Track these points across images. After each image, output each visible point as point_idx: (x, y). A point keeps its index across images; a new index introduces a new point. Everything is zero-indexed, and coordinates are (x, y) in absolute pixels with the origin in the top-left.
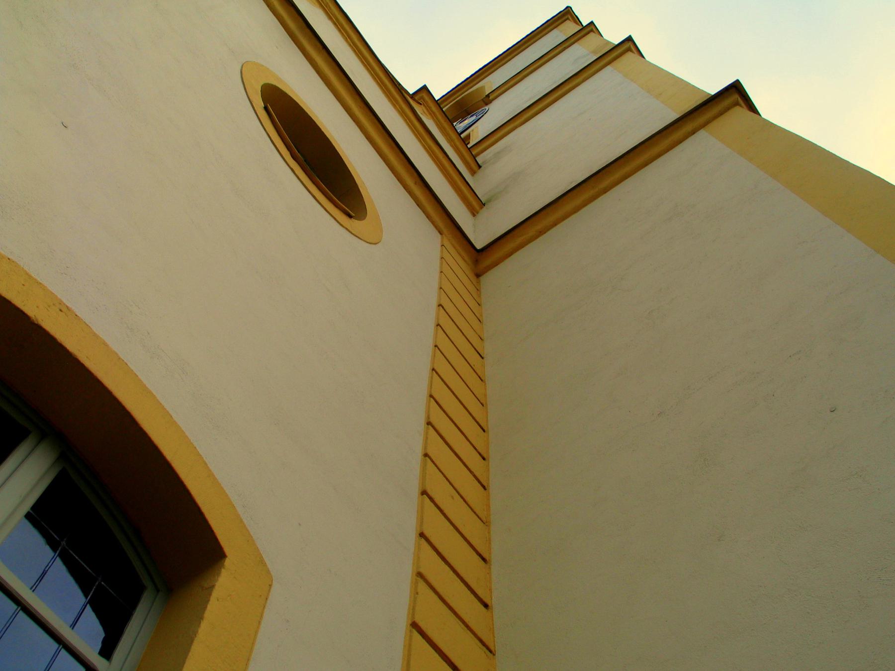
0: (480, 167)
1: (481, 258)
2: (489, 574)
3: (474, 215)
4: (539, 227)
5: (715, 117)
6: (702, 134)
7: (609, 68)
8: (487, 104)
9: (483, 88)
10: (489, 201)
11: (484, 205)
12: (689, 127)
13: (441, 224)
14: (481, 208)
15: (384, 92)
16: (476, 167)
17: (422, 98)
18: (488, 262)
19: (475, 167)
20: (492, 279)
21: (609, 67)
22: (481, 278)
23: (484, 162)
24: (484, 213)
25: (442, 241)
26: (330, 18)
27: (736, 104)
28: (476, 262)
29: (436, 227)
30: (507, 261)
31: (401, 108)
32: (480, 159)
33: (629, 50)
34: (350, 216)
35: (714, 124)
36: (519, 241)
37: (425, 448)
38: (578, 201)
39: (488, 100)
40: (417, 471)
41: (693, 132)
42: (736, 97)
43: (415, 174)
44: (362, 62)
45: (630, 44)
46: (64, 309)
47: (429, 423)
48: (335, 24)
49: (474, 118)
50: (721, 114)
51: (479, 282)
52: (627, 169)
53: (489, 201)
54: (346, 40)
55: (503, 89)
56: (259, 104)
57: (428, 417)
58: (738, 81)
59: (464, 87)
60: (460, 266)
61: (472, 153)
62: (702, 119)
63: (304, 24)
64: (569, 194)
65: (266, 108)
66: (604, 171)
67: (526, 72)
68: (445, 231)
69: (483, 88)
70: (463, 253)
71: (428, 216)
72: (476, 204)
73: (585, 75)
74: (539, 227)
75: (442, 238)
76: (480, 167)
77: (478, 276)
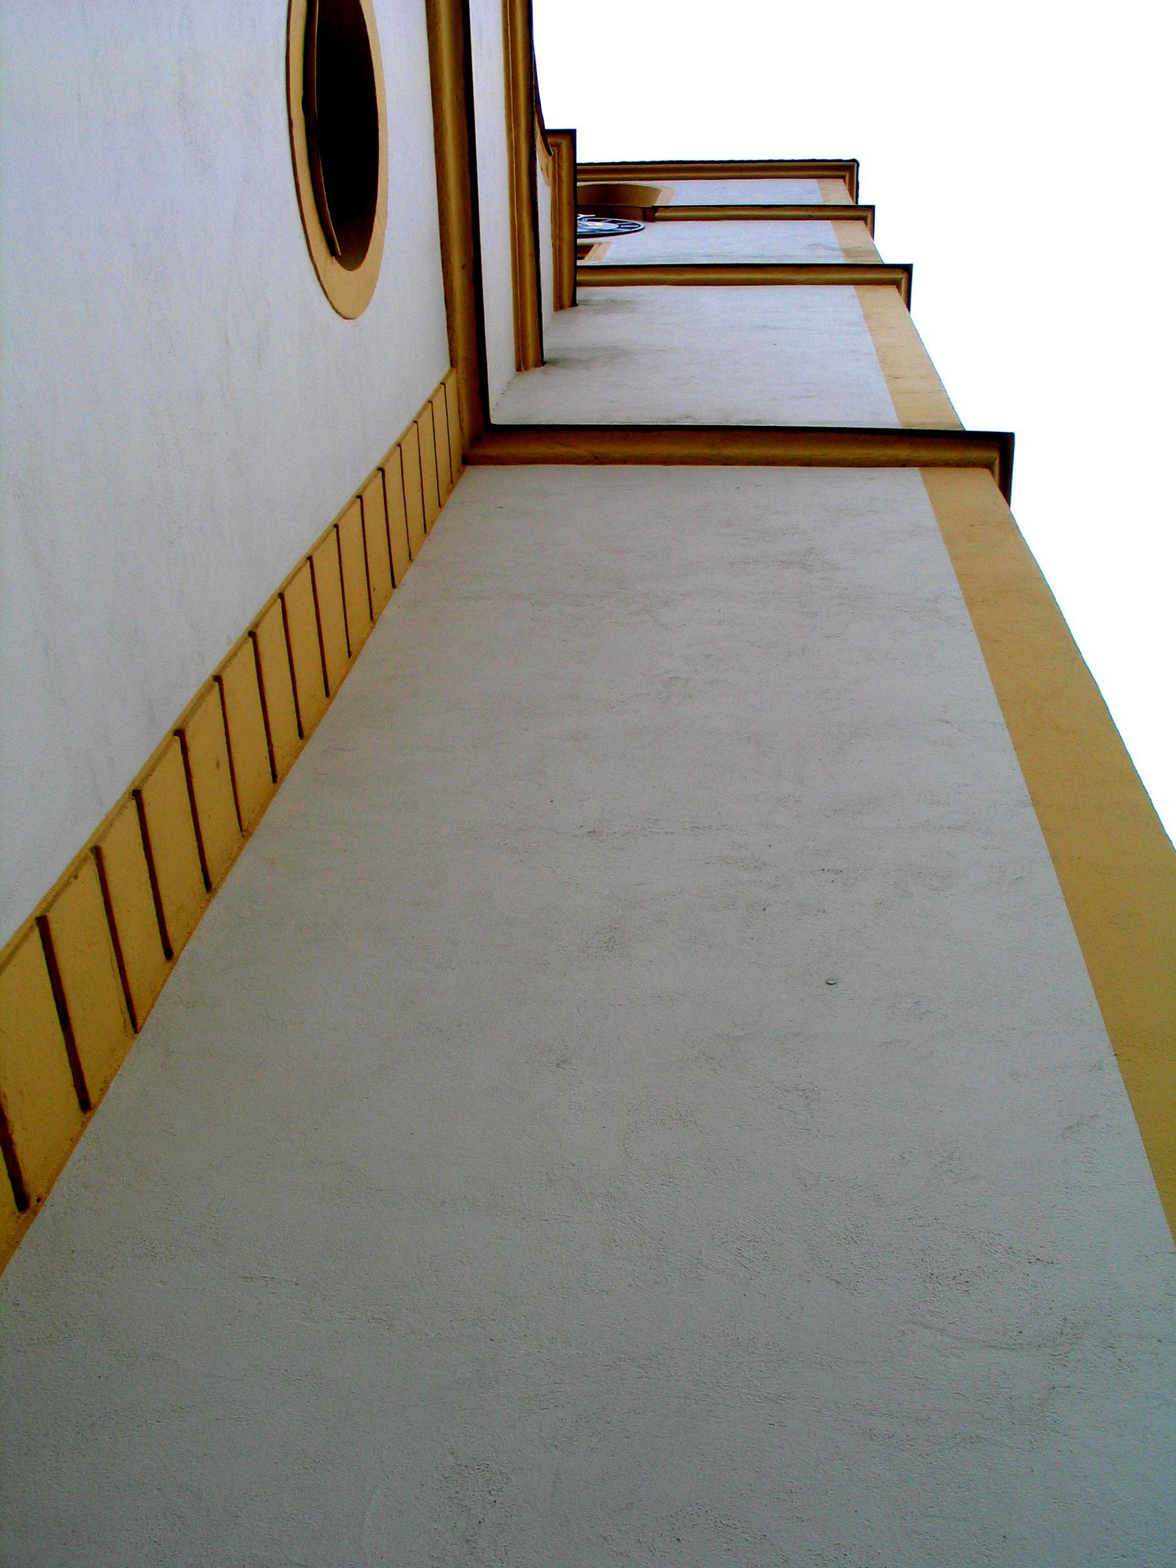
0: (574, 303)
1: (485, 440)
2: (203, 909)
3: (519, 369)
9: (656, 191)
10: (554, 363)
16: (566, 301)
17: (558, 146)
19: (566, 299)
20: (486, 482)
22: (469, 468)
23: (586, 302)
25: (447, 376)
32: (581, 293)
36: (560, 450)
39: (651, 214)
41: (904, 464)
42: (994, 455)
49: (614, 226)
51: (460, 472)
53: (554, 363)
55: (673, 214)
60: (448, 430)
69: (656, 191)
72: (531, 354)
75: (450, 372)
76: (574, 303)
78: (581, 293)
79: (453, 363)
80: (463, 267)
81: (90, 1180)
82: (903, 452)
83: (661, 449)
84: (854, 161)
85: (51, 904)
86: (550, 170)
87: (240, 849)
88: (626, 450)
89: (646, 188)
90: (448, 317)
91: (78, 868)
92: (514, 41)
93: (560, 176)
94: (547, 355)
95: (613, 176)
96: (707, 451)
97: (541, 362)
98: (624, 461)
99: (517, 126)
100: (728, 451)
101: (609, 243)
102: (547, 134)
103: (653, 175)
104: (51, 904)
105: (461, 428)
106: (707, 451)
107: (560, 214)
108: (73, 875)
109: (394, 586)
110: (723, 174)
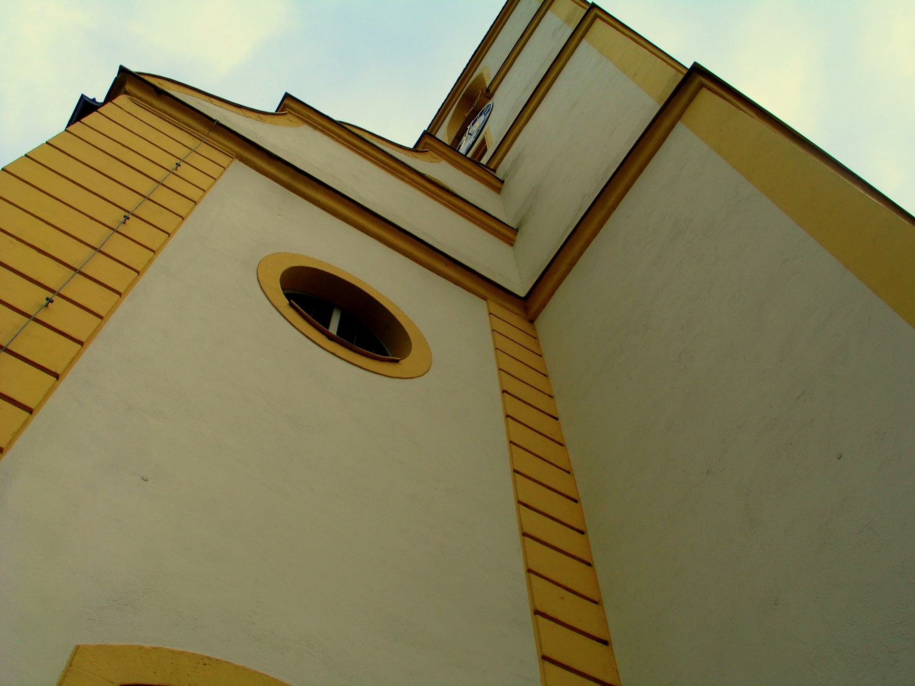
0: (502, 182)
1: (528, 305)
2: (613, 654)
3: (512, 245)
4: (568, 260)
6: (680, 127)
7: (584, 42)
8: (490, 98)
10: (520, 225)
11: (517, 230)
12: (667, 123)
13: (482, 291)
14: (516, 235)
15: (389, 171)
16: (497, 185)
17: (427, 144)
18: (535, 306)
23: (505, 175)
24: (520, 239)
25: (488, 308)
26: (316, 128)
27: (702, 86)
28: (526, 309)
32: (500, 174)
33: (596, 16)
34: (397, 361)
36: (556, 277)
37: (526, 563)
39: (489, 94)
40: (524, 588)
41: (672, 126)
45: (596, 11)
46: (207, 661)
47: (524, 534)
49: (482, 118)
50: (691, 100)
51: (534, 329)
52: (626, 180)
53: (520, 225)
55: (497, 82)
56: (283, 301)
58: (695, 63)
59: (464, 79)
60: (512, 317)
62: (676, 111)
64: (584, 220)
65: (291, 305)
66: (607, 189)
67: (514, 55)
68: (488, 295)
69: (481, 75)
70: (509, 306)
71: (469, 290)
72: (507, 233)
73: (565, 56)
74: (568, 260)
75: (488, 304)
76: (502, 182)
77: (532, 321)
78: (500, 174)
79: (485, 299)
81: (7, 456)
83: (587, 232)
85: (522, 528)
86: (436, 156)
87: (604, 612)
89: (477, 78)
91: (544, 669)
92: (372, 156)
94: (513, 225)
96: (603, 213)
97: (516, 231)
98: (581, 253)
102: (417, 149)
104: (522, 528)
106: (603, 213)
108: (507, 424)
109: (557, 419)
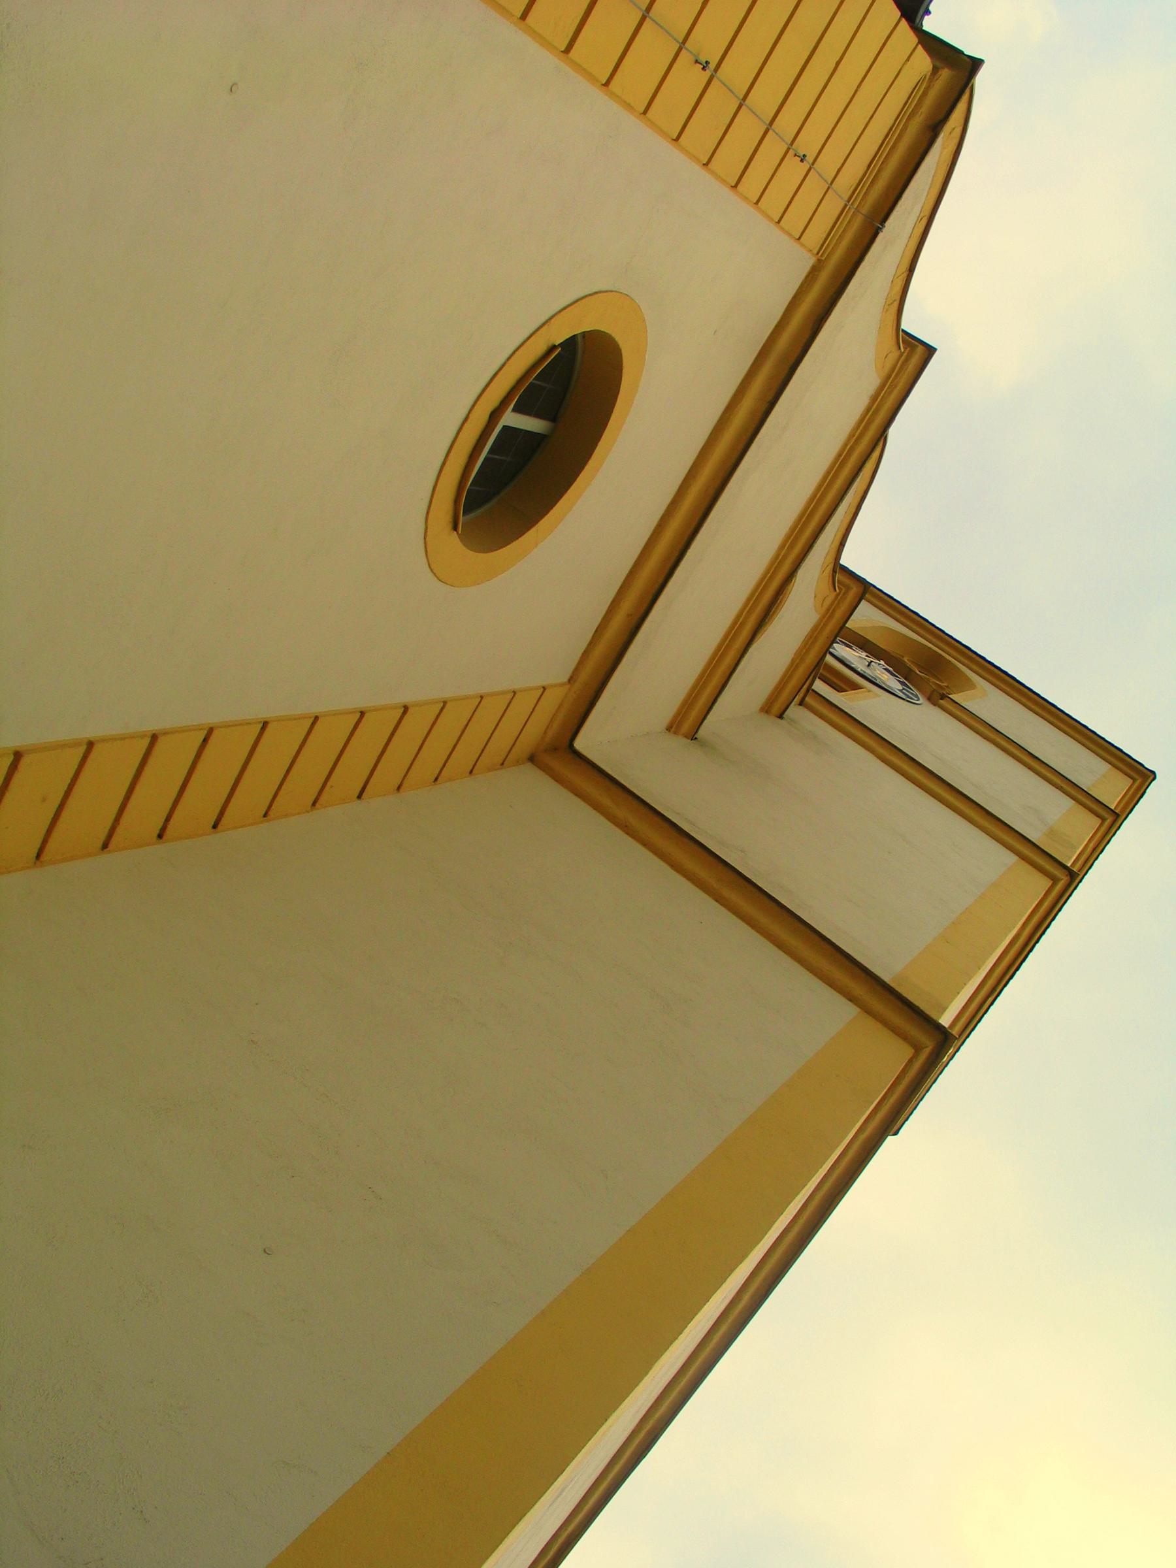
0: (781, 716)
1: (560, 752)
5: (885, 1023)
6: (851, 1011)
8: (929, 699)
9: (968, 685)
10: (704, 744)
11: (694, 738)
13: (584, 676)
17: (848, 588)
19: (776, 708)
20: (533, 781)
21: (1015, 858)
22: (529, 765)
24: (678, 743)
26: (874, 399)
28: (553, 749)
29: (577, 670)
30: (565, 793)
31: (785, 557)
32: (794, 711)
34: (455, 528)
35: (870, 1022)
36: (606, 801)
37: (104, 740)
38: (690, 865)
39: (938, 698)
41: (852, 999)
42: (929, 1046)
43: (642, 610)
44: (828, 472)
48: (868, 410)
51: (518, 762)
52: (764, 920)
53: (704, 744)
54: (851, 436)
57: (166, 733)
61: (804, 695)
63: (793, 360)
68: (577, 686)
71: (586, 654)
72: (689, 721)
75: (562, 685)
76: (781, 716)
77: (532, 759)
78: (794, 711)
79: (571, 680)
80: (628, 615)
82: (858, 989)
84: (1153, 773)
88: (655, 837)
90: (590, 643)
93: (834, 611)
95: (959, 657)
98: (645, 844)
99: (792, 547)
100: (726, 892)
101: (877, 695)
103: (983, 673)
105: (545, 733)
107: (814, 642)
109: (359, 797)
110: (1040, 711)
